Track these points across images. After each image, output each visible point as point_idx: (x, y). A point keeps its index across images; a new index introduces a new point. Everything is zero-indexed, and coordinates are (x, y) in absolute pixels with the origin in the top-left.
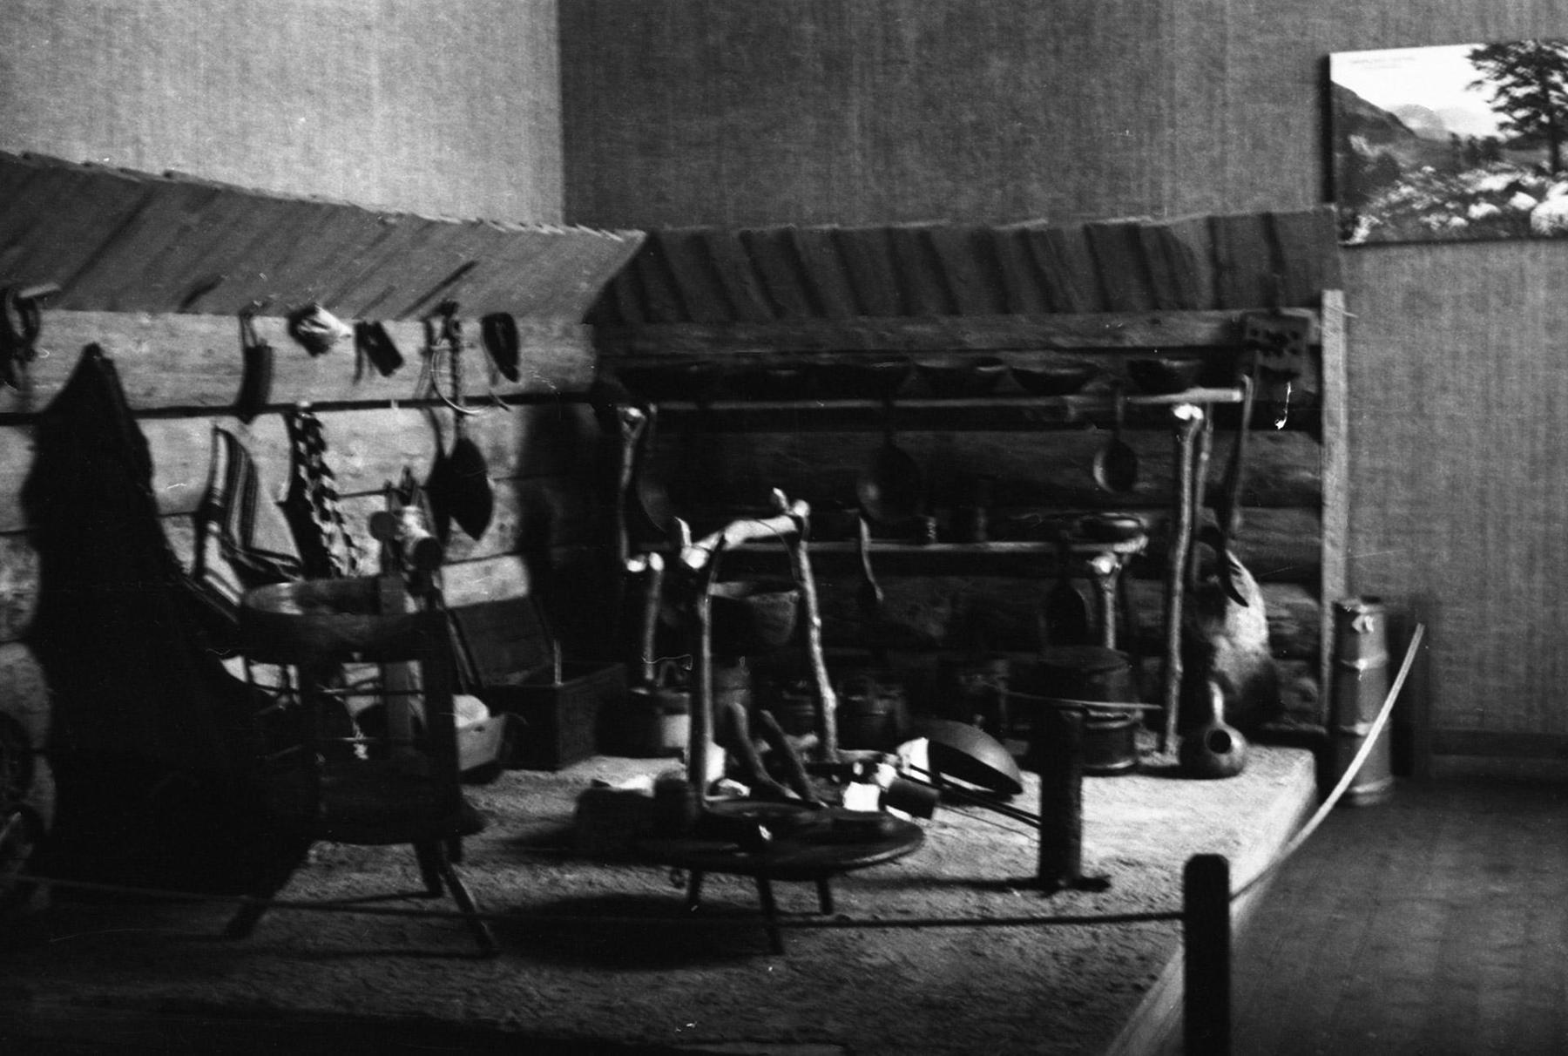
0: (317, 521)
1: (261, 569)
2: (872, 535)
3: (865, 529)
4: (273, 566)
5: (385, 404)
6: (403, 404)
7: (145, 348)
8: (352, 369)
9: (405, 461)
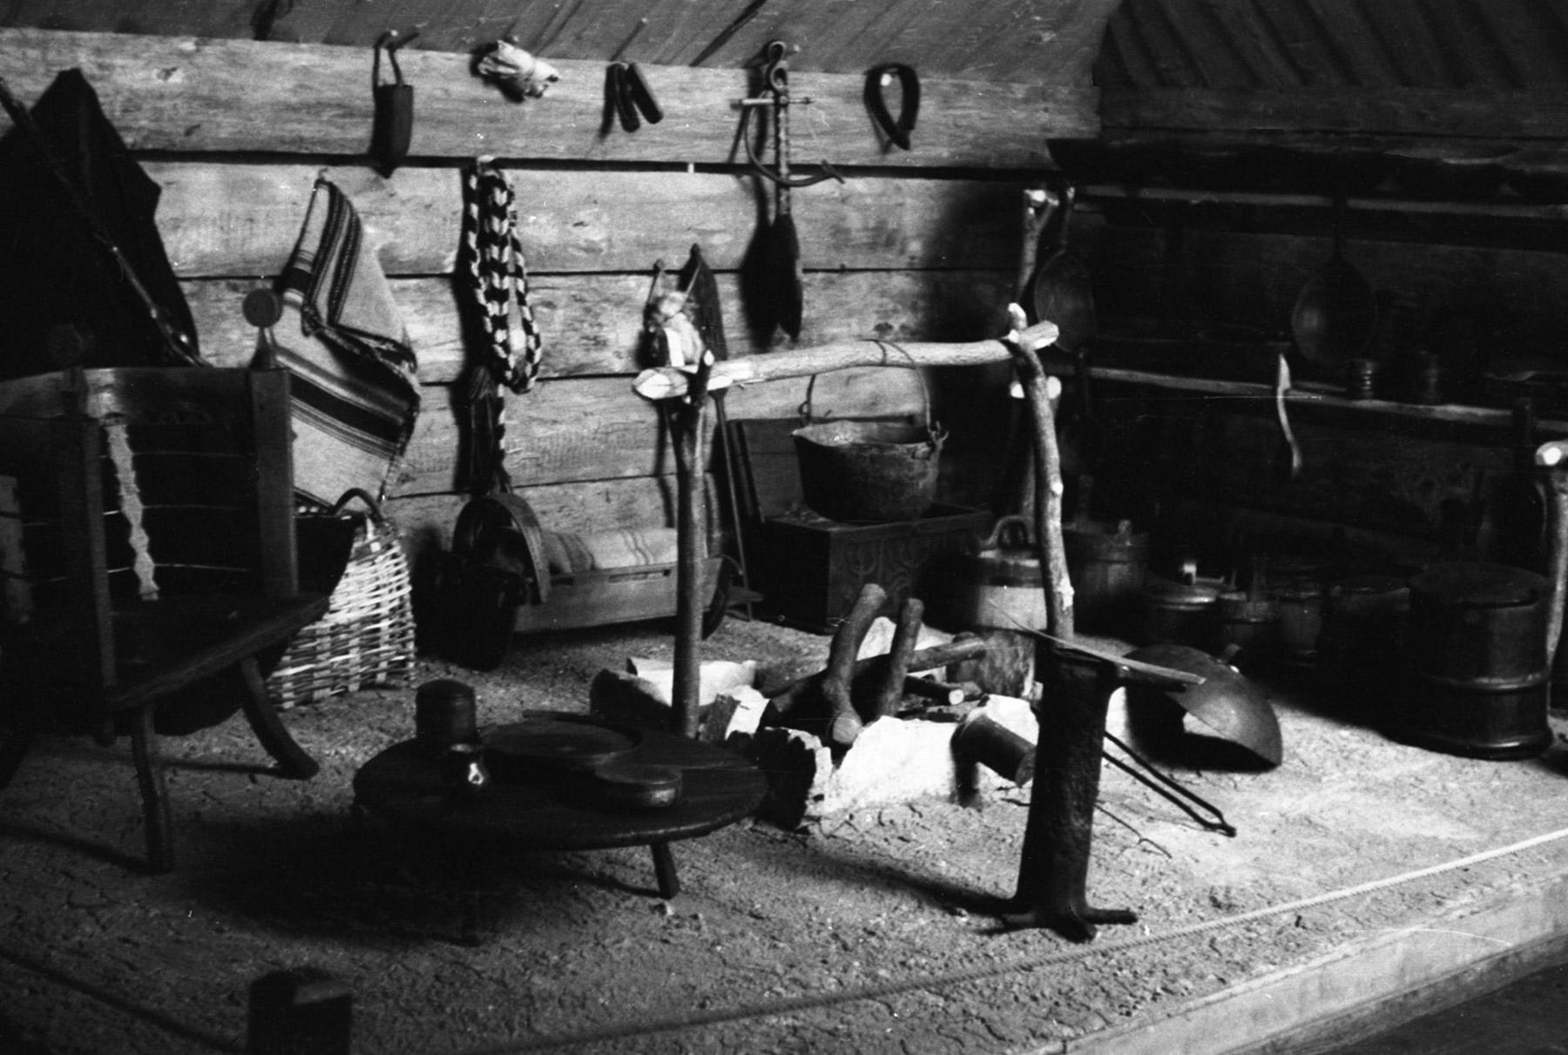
0: (482, 300)
1: (356, 351)
2: (1294, 376)
3: (1284, 369)
4: (366, 348)
5: (680, 166)
6: (702, 168)
7: (177, 79)
8: (598, 121)
9: (691, 238)
